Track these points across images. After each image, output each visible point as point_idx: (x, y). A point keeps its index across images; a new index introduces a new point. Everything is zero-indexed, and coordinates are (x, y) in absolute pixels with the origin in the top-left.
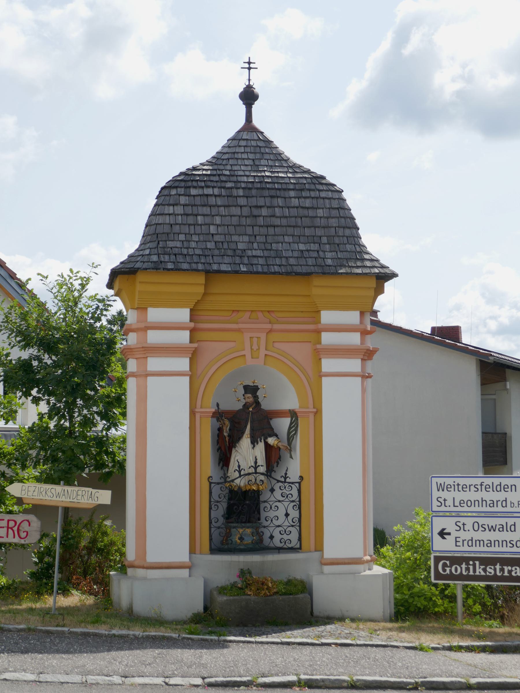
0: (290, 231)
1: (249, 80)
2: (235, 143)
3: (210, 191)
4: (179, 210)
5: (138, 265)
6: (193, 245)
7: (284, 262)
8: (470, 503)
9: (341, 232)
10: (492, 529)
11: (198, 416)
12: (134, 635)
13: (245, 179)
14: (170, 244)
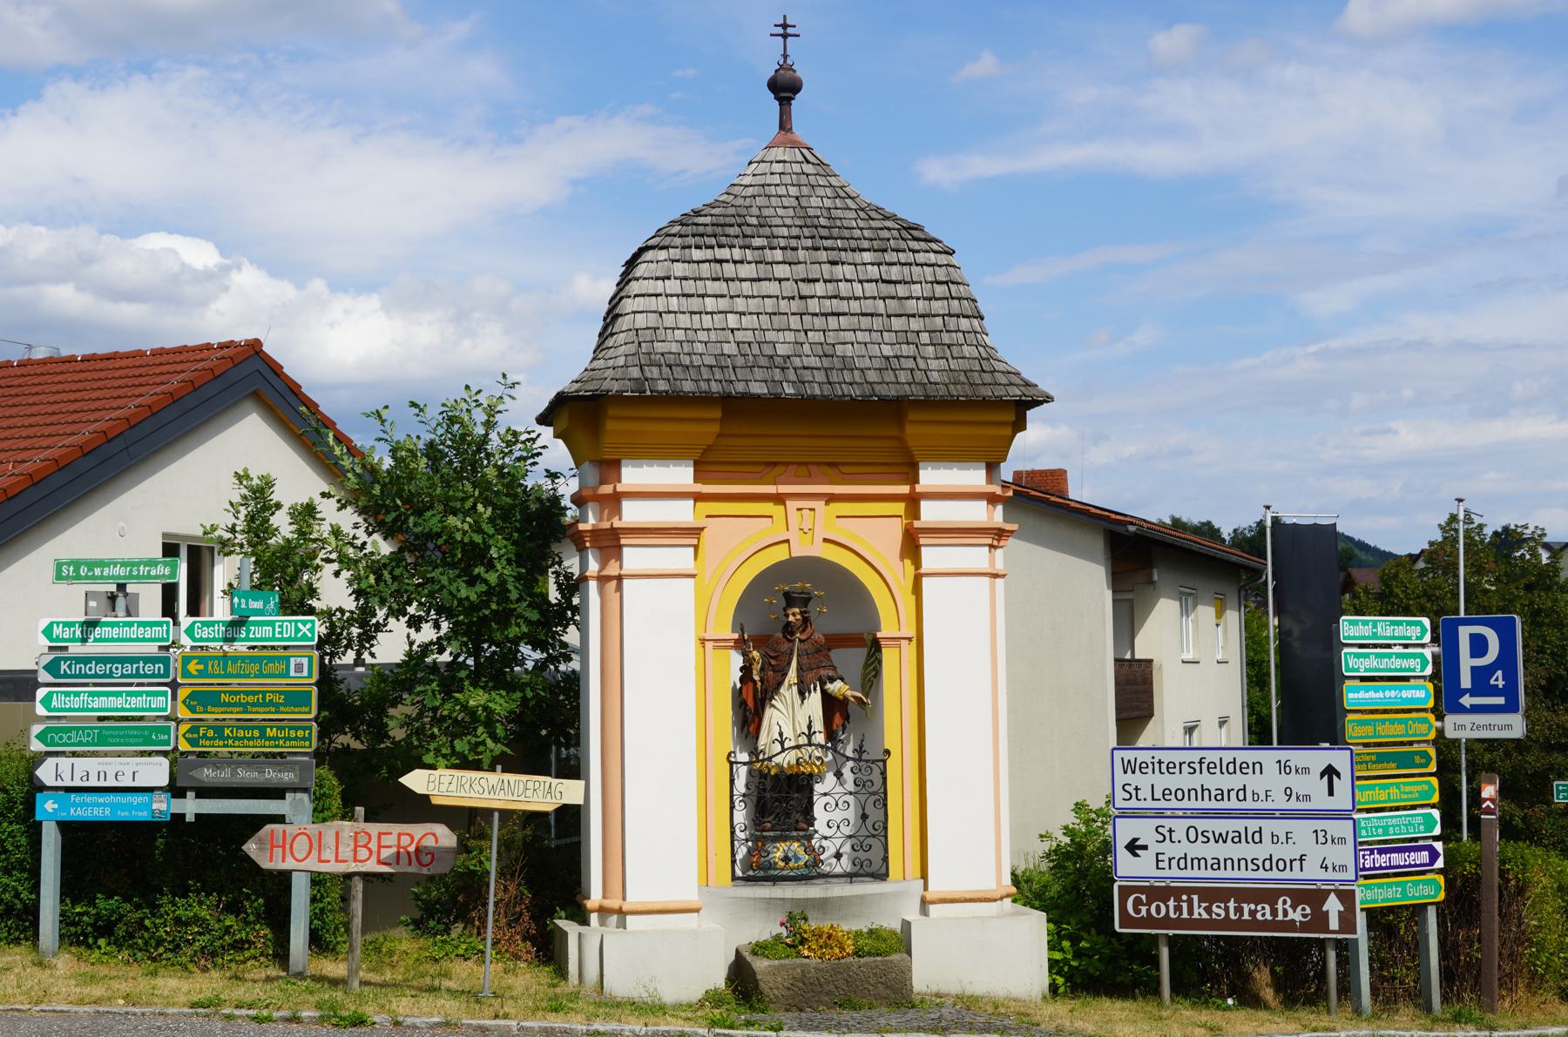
1: (785, 56)
4: (673, 286)
6: (700, 348)
10: (1221, 838)
13: (785, 231)
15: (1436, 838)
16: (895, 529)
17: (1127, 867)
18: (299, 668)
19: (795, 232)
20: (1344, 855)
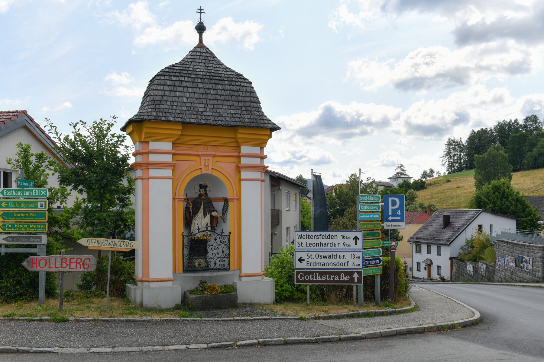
0: (226, 103)
1: (201, 19)
2: (194, 53)
3: (183, 79)
4: (166, 88)
5: (145, 117)
6: (175, 107)
7: (223, 119)
8: (315, 244)
9: (252, 105)
10: (325, 257)
11: (176, 200)
12: (156, 320)
13: (201, 73)
14: (162, 107)
15: (380, 256)
16: (233, 166)
17: (299, 266)
18: (41, 205)
19: (204, 73)
20: (359, 261)
